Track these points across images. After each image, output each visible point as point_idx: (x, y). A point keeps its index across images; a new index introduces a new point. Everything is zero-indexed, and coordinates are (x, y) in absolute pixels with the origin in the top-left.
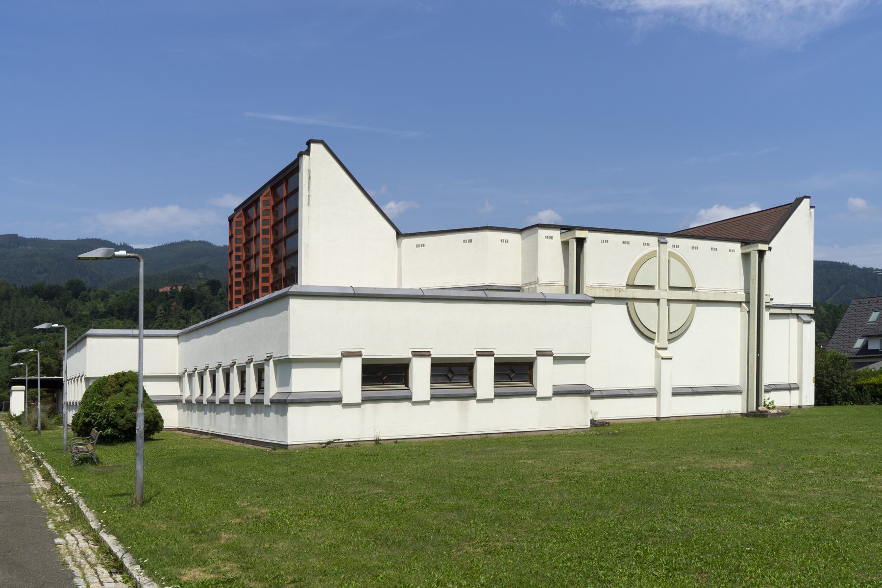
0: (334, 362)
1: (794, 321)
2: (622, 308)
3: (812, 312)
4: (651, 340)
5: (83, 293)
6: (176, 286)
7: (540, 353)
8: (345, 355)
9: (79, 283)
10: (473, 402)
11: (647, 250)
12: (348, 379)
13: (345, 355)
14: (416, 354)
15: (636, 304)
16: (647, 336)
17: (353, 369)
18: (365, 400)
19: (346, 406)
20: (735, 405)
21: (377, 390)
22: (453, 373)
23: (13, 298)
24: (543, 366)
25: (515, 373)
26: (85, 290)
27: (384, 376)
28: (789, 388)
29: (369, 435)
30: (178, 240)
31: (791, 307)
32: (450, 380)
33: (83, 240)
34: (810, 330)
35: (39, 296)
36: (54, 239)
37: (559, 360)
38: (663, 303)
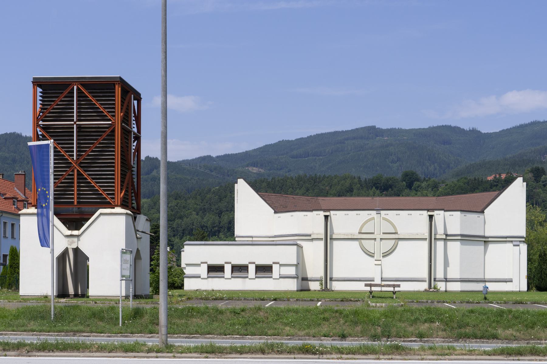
0: (198, 265)
1: (511, 245)
2: (356, 243)
3: (524, 240)
4: (373, 257)
5: (416, 184)
6: (500, 175)
7: (274, 263)
8: (202, 263)
9: (413, 174)
10: (247, 279)
11: (370, 217)
12: (203, 270)
13: (202, 263)
14: (226, 263)
15: (362, 241)
16: (371, 255)
17: (205, 267)
18: (208, 277)
19: (202, 279)
20: (424, 286)
21: (212, 274)
22: (240, 269)
23: (355, 191)
24: (275, 268)
25: (264, 270)
26: (418, 180)
27: (215, 269)
28: (506, 281)
29: (210, 288)
30: (527, 121)
31: (506, 238)
32: (240, 272)
33: (434, 128)
34: (524, 248)
35: (377, 188)
36: (407, 128)
37: (281, 265)
38: (378, 240)
